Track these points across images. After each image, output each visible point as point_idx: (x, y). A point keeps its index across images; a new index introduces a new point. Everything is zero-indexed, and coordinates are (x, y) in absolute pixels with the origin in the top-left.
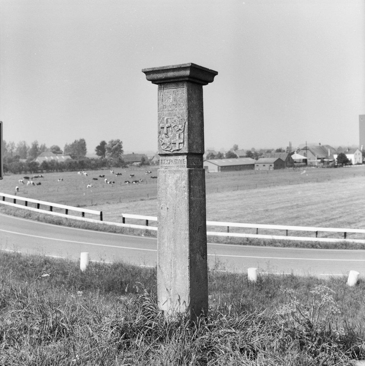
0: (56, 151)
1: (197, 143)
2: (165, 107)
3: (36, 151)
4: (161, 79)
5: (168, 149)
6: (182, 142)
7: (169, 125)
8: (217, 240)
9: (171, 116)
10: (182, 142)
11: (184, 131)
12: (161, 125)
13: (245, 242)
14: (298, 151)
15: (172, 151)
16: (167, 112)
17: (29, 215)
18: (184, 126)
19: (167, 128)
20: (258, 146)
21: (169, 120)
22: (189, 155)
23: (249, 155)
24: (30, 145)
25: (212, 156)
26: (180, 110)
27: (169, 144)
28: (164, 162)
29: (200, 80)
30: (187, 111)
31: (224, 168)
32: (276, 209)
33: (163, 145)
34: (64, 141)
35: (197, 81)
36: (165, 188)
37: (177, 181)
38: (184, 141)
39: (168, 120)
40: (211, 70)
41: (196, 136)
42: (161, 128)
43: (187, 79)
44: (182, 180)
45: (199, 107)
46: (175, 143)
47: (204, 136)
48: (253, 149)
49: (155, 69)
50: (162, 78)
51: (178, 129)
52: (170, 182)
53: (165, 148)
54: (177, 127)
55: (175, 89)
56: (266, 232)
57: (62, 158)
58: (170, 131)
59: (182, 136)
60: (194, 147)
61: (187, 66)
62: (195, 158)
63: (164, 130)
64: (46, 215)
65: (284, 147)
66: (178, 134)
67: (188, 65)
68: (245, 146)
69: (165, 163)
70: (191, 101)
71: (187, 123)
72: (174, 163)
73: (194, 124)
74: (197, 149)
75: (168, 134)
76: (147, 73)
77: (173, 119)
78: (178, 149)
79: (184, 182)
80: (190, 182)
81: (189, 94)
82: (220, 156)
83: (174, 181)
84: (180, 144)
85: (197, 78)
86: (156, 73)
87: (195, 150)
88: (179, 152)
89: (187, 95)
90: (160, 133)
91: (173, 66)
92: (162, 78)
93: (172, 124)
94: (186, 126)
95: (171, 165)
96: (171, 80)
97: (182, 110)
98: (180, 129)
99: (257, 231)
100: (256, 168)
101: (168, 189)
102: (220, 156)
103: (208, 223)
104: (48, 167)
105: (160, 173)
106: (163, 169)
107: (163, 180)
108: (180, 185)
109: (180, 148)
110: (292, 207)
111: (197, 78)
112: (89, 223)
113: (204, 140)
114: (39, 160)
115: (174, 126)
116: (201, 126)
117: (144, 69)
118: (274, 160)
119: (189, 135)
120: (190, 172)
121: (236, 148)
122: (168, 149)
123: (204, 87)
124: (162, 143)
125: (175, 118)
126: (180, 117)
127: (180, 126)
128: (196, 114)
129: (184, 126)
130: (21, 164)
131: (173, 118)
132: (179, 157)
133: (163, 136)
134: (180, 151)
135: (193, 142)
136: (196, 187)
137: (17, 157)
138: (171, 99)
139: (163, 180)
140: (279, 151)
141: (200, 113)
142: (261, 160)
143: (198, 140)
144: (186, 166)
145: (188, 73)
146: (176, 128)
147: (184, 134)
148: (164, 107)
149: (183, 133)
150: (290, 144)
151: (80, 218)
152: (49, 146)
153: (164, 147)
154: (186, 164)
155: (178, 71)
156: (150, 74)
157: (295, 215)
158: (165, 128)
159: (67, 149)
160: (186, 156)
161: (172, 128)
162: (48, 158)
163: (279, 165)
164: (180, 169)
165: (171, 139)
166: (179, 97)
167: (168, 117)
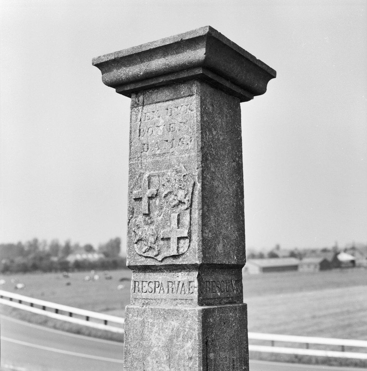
0: (89, 249)
1: (226, 237)
2: (145, 147)
3: (68, 249)
4: (136, 80)
5: (150, 254)
6: (186, 234)
7: (153, 190)
8: (260, 356)
9: (160, 169)
10: (186, 234)
11: (191, 206)
12: (135, 192)
13: (294, 359)
14: (345, 251)
15: (160, 258)
16: (150, 160)
17: (45, 321)
18: (192, 193)
19: (150, 198)
20: (301, 245)
21: (155, 180)
22: (205, 269)
23: (293, 255)
24: (62, 243)
25: (253, 256)
26: (181, 152)
27: (152, 239)
28: (140, 286)
29: (234, 81)
30: (200, 154)
31: (266, 270)
32: (325, 316)
33: (140, 243)
34: (99, 240)
35: (228, 84)
36: (141, 357)
37: (171, 340)
38: (190, 233)
39: (153, 179)
40: (259, 61)
41: (223, 221)
42: (135, 199)
43: (199, 71)
44: (186, 338)
45: (233, 149)
46: (168, 239)
47: (243, 221)
48: (296, 249)
49: (121, 55)
50: (138, 78)
51: (176, 202)
52: (154, 342)
53: (143, 250)
54: (173, 196)
55: (171, 102)
56: (317, 346)
57: (94, 257)
58: (156, 206)
59: (186, 220)
60: (220, 248)
61: (198, 35)
62: (221, 278)
63: (142, 202)
64: (65, 322)
65: (330, 245)
66: (176, 215)
67: (202, 33)
68: (288, 245)
69: (144, 290)
70: (210, 131)
71: (199, 186)
72: (166, 291)
73: (219, 190)
74: (227, 255)
75: (151, 215)
76: (104, 66)
77: (165, 178)
78: (175, 253)
79: (189, 345)
80: (207, 345)
81: (204, 112)
82: (261, 256)
83: (163, 339)
84: (182, 241)
85: (226, 75)
86: (125, 66)
87: (222, 253)
88: (178, 262)
89: (199, 113)
90: (133, 213)
91: (164, 40)
92: (138, 78)
93: (162, 189)
94: (196, 193)
95: (157, 295)
96: (161, 80)
97: (187, 153)
98: (180, 202)
99: (308, 346)
100: (300, 270)
101: (149, 358)
102: (261, 256)
103: (251, 335)
104: (80, 266)
105: (131, 315)
106: (137, 306)
107: (136, 333)
108: (180, 352)
109: (181, 251)
110: (342, 313)
111: (226, 75)
112: (113, 333)
113: (244, 231)
114: (71, 259)
115: (166, 193)
116: (237, 195)
117: (96, 56)
118: (318, 260)
119: (204, 216)
120: (205, 315)
121: (278, 247)
122: (150, 254)
123: (241, 103)
124: (138, 238)
125: (170, 173)
126: (180, 171)
127: (181, 193)
128: (223, 165)
129: (192, 193)
130: (52, 263)
131: (164, 174)
132: (180, 274)
133: (140, 218)
134: (181, 259)
135: (216, 237)
136: (222, 354)
137: (48, 255)
138: (161, 128)
139: (136, 333)
140: (325, 251)
141: (234, 164)
142: (306, 260)
143: (230, 229)
144: (196, 300)
145: (199, 54)
146: (171, 199)
147: (191, 213)
148: (145, 146)
149: (188, 211)
150: (336, 243)
151: (102, 326)
152: (82, 244)
153: (141, 248)
154: (196, 295)
155: (177, 53)
156: (110, 70)
157: (346, 322)
158: (145, 200)
159: (101, 248)
160: (196, 274)
161: (160, 200)
162: (79, 257)
163: (325, 266)
164: (179, 307)
165: (157, 227)
166: (180, 120)
167: (152, 172)
